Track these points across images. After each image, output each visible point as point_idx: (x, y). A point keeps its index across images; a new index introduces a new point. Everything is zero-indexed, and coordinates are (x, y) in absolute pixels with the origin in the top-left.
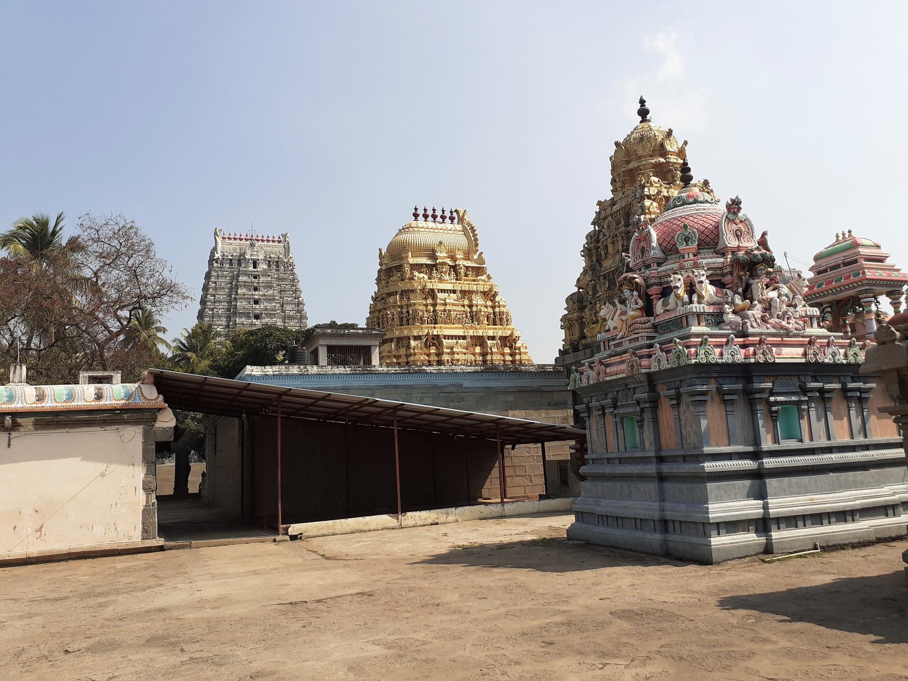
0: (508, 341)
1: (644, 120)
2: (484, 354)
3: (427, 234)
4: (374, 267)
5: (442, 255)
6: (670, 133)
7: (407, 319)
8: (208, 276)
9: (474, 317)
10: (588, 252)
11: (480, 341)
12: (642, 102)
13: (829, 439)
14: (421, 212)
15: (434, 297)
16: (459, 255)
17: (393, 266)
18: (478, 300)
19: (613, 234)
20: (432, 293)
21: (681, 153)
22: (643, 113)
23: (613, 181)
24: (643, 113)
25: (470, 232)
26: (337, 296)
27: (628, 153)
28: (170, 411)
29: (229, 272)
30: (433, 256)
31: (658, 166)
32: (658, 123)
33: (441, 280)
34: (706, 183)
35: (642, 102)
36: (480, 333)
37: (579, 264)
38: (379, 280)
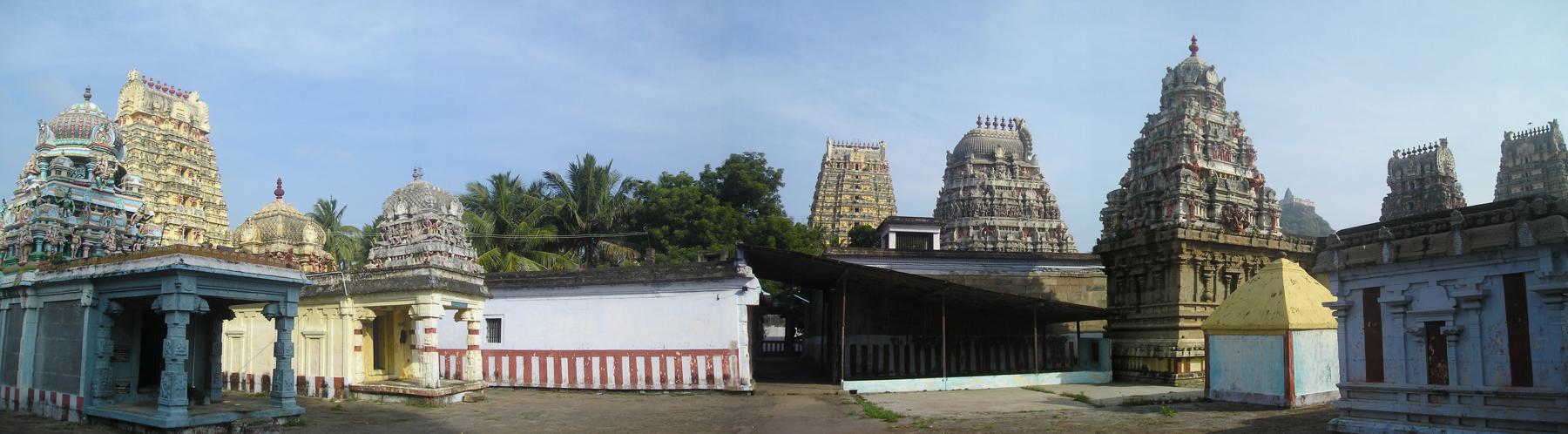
0: (1058, 231)
1: (1193, 55)
2: (1035, 244)
3: (989, 135)
4: (943, 165)
5: (1000, 154)
6: (1212, 69)
7: (968, 211)
8: (820, 176)
9: (1027, 211)
10: (1134, 156)
11: (1031, 231)
12: (1194, 40)
13: (1485, 384)
14: (984, 120)
15: (992, 194)
16: (1015, 156)
17: (957, 162)
18: (1031, 195)
19: (1158, 150)
20: (989, 189)
21: (1219, 86)
22: (1194, 49)
23: (1162, 100)
24: (1194, 49)
25: (1024, 137)
26: (917, 193)
27: (1176, 79)
28: (756, 280)
29: (838, 172)
30: (992, 156)
31: (1199, 92)
32: (1203, 58)
33: (999, 178)
34: (1236, 114)
35: (1194, 40)
36: (1029, 225)
37: (1128, 165)
38: (945, 178)
